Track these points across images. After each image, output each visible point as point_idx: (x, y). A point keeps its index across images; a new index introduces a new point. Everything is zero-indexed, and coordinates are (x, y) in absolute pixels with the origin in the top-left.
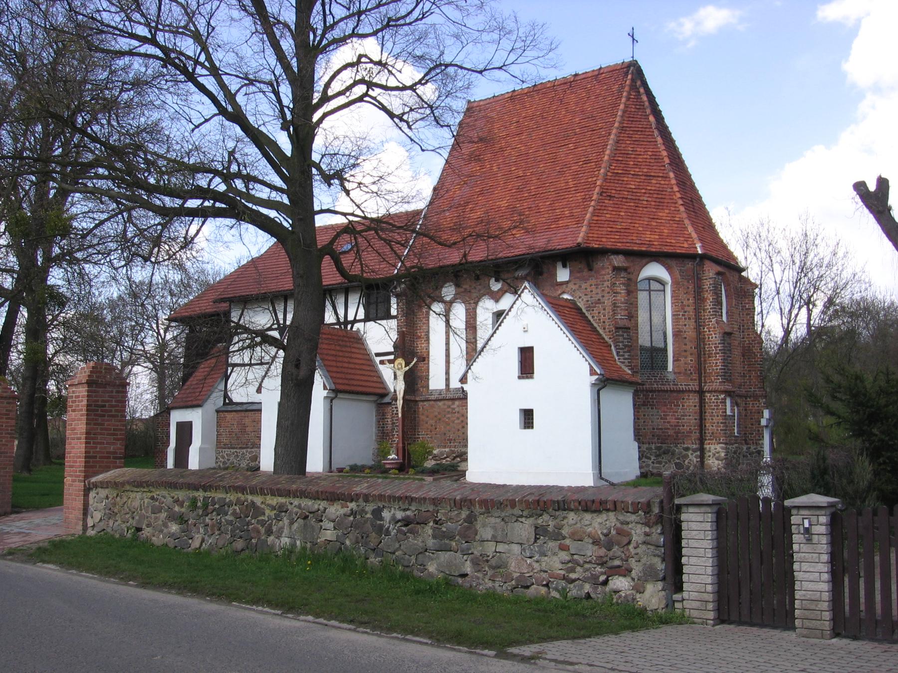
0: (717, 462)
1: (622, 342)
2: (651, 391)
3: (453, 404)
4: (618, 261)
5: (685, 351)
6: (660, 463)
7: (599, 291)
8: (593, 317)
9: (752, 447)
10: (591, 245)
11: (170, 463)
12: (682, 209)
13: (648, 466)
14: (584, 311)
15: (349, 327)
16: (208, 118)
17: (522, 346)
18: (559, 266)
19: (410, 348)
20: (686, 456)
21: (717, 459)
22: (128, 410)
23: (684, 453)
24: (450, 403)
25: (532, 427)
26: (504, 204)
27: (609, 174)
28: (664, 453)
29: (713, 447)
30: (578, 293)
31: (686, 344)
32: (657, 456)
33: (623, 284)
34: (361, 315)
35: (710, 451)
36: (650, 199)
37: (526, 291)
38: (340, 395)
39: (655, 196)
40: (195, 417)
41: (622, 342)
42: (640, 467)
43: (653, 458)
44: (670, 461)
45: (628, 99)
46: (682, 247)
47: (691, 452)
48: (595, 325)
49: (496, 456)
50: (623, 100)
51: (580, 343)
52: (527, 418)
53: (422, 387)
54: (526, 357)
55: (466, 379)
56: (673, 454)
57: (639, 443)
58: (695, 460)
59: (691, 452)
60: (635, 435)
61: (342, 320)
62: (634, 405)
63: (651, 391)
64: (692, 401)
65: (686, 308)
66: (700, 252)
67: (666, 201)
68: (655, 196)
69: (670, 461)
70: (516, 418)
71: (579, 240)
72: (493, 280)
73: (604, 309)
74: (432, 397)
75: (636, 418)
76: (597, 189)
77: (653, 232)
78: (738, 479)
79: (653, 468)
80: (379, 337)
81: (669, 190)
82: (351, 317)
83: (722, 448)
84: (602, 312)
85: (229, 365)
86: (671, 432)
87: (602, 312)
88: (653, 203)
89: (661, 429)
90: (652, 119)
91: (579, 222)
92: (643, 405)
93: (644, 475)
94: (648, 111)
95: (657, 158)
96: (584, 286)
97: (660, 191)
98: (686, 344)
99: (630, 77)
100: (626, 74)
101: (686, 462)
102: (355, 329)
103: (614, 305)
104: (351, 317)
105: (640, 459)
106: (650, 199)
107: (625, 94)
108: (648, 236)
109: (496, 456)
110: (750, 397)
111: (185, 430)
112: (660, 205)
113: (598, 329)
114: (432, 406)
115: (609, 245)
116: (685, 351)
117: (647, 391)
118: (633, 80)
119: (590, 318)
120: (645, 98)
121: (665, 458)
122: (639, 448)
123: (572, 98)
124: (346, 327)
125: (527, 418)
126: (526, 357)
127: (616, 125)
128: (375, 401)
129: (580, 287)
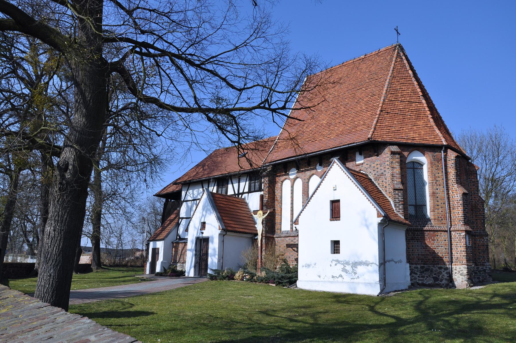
0: (461, 277)
1: (398, 198)
2: (417, 231)
3: (295, 239)
4: (395, 148)
5: (438, 205)
6: (423, 277)
7: (382, 168)
8: (379, 184)
9: (480, 267)
10: (377, 139)
11: (148, 272)
12: (431, 120)
13: (415, 279)
14: (373, 180)
15: (240, 196)
16: (387, 264)
17: (333, 199)
18: (357, 155)
19: (270, 204)
20: (440, 273)
21: (461, 275)
22: (490, 256)
23: (439, 270)
24: (293, 238)
25: (339, 253)
26: (324, 122)
27: (386, 100)
28: (426, 270)
29: (458, 267)
30: (369, 170)
31: (438, 201)
32: (421, 272)
33: (397, 162)
34: (246, 190)
35: (456, 270)
36: (411, 114)
37: (335, 164)
38: (228, 233)
39: (415, 113)
40: (160, 245)
41: (398, 198)
42: (411, 280)
43: (419, 274)
44: (430, 276)
45: (396, 62)
46: (435, 142)
47: (443, 270)
48: (380, 189)
49: (318, 274)
50: (393, 62)
51: (371, 296)
52: (336, 246)
53: (278, 229)
54: (335, 205)
55: (298, 221)
56: (432, 271)
57: (410, 264)
58: (446, 275)
59: (443, 270)
60: (407, 259)
61: (236, 193)
62: (406, 239)
63: (417, 231)
64: (444, 236)
65: (438, 179)
66: (445, 144)
67: (421, 115)
68: (415, 113)
69: (430, 276)
70: (328, 247)
71: (369, 136)
72: (318, 164)
73: (386, 179)
74: (283, 235)
75: (408, 248)
76: (380, 109)
77: (415, 132)
78: (121, 168)
79: (419, 280)
80: (254, 201)
81: (423, 110)
82: (241, 191)
83: (465, 268)
84: (384, 180)
85: (180, 218)
86: (430, 257)
87: (384, 180)
88: (414, 117)
89: (424, 255)
90: (410, 72)
91: (369, 127)
92: (412, 239)
93: (412, 284)
94: (408, 68)
95: (414, 92)
96: (373, 165)
97: (418, 110)
98: (438, 201)
99: (396, 51)
100: (394, 50)
101: (441, 276)
102: (243, 197)
103: (392, 175)
104: (241, 191)
105: (410, 274)
106: (411, 114)
107: (394, 59)
108: (412, 135)
109: (318, 274)
110: (477, 236)
111: (155, 252)
112: (418, 118)
113: (382, 191)
114: (283, 241)
115: (388, 139)
116: (438, 205)
117: (414, 230)
118: (398, 53)
119: (377, 185)
120: (405, 61)
121: (427, 274)
122: (410, 267)
123: (364, 66)
124: (238, 196)
125: (336, 246)
126: (335, 205)
127: (390, 75)
128: (251, 238)
129: (370, 166)
